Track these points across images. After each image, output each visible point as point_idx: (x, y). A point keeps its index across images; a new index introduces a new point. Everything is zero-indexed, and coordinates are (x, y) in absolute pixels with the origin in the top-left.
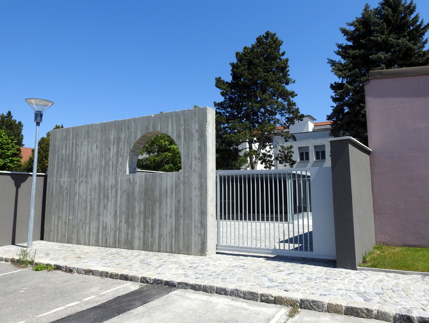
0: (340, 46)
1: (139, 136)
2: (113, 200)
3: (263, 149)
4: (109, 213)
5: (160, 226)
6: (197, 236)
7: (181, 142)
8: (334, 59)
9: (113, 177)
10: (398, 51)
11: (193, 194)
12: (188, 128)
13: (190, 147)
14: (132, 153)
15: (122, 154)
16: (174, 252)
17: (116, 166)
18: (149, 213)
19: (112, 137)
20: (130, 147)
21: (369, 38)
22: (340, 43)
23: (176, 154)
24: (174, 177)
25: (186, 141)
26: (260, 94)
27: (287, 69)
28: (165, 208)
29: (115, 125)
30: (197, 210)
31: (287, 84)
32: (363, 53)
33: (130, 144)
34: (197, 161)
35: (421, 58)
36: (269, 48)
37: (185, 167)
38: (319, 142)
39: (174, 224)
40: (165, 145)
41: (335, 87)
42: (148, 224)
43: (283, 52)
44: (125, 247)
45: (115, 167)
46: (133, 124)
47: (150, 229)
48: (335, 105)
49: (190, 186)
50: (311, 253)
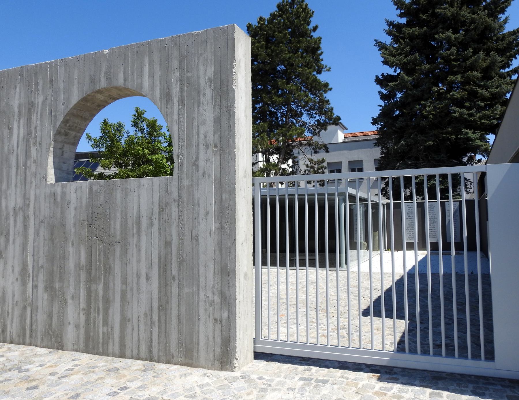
0: (391, 24)
1: (75, 99)
2: (19, 241)
3: (284, 163)
4: (9, 268)
5: (124, 299)
6: (211, 325)
7: (172, 108)
8: (383, 41)
9: (18, 190)
10: (473, 29)
11: (202, 226)
12: (189, 75)
13: (193, 119)
14: (60, 138)
15: (38, 139)
16: (156, 358)
17: (25, 165)
18: (97, 270)
19: (15, 103)
20: (55, 123)
21: (434, 12)
22: (391, 19)
23: (160, 167)
24: (156, 188)
25: (184, 105)
26: (283, 83)
27: (319, 52)
28: (135, 259)
29: (21, 75)
30: (211, 265)
31: (319, 72)
32: (425, 31)
33: (55, 116)
34: (210, 153)
35: (500, 42)
36: (296, 19)
37: (181, 166)
38: (356, 155)
39: (156, 296)
40: (144, 155)
41: (383, 81)
42: (97, 293)
43: (314, 26)
44: (45, 344)
45: (22, 169)
46: (62, 71)
47: (101, 306)
48: (383, 104)
49: (193, 209)
50: (488, 364)
